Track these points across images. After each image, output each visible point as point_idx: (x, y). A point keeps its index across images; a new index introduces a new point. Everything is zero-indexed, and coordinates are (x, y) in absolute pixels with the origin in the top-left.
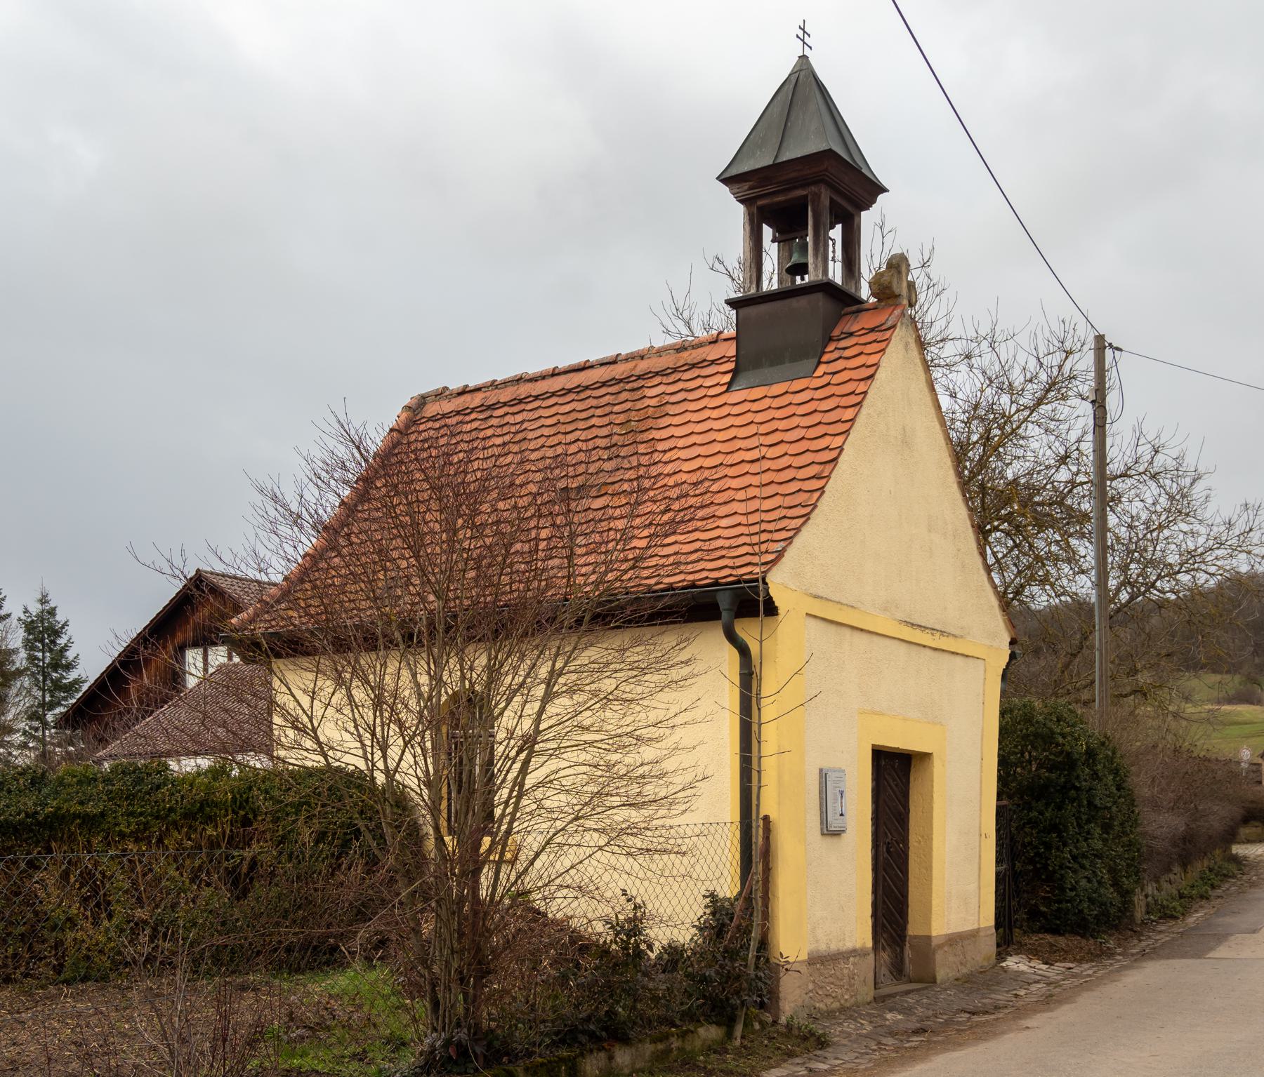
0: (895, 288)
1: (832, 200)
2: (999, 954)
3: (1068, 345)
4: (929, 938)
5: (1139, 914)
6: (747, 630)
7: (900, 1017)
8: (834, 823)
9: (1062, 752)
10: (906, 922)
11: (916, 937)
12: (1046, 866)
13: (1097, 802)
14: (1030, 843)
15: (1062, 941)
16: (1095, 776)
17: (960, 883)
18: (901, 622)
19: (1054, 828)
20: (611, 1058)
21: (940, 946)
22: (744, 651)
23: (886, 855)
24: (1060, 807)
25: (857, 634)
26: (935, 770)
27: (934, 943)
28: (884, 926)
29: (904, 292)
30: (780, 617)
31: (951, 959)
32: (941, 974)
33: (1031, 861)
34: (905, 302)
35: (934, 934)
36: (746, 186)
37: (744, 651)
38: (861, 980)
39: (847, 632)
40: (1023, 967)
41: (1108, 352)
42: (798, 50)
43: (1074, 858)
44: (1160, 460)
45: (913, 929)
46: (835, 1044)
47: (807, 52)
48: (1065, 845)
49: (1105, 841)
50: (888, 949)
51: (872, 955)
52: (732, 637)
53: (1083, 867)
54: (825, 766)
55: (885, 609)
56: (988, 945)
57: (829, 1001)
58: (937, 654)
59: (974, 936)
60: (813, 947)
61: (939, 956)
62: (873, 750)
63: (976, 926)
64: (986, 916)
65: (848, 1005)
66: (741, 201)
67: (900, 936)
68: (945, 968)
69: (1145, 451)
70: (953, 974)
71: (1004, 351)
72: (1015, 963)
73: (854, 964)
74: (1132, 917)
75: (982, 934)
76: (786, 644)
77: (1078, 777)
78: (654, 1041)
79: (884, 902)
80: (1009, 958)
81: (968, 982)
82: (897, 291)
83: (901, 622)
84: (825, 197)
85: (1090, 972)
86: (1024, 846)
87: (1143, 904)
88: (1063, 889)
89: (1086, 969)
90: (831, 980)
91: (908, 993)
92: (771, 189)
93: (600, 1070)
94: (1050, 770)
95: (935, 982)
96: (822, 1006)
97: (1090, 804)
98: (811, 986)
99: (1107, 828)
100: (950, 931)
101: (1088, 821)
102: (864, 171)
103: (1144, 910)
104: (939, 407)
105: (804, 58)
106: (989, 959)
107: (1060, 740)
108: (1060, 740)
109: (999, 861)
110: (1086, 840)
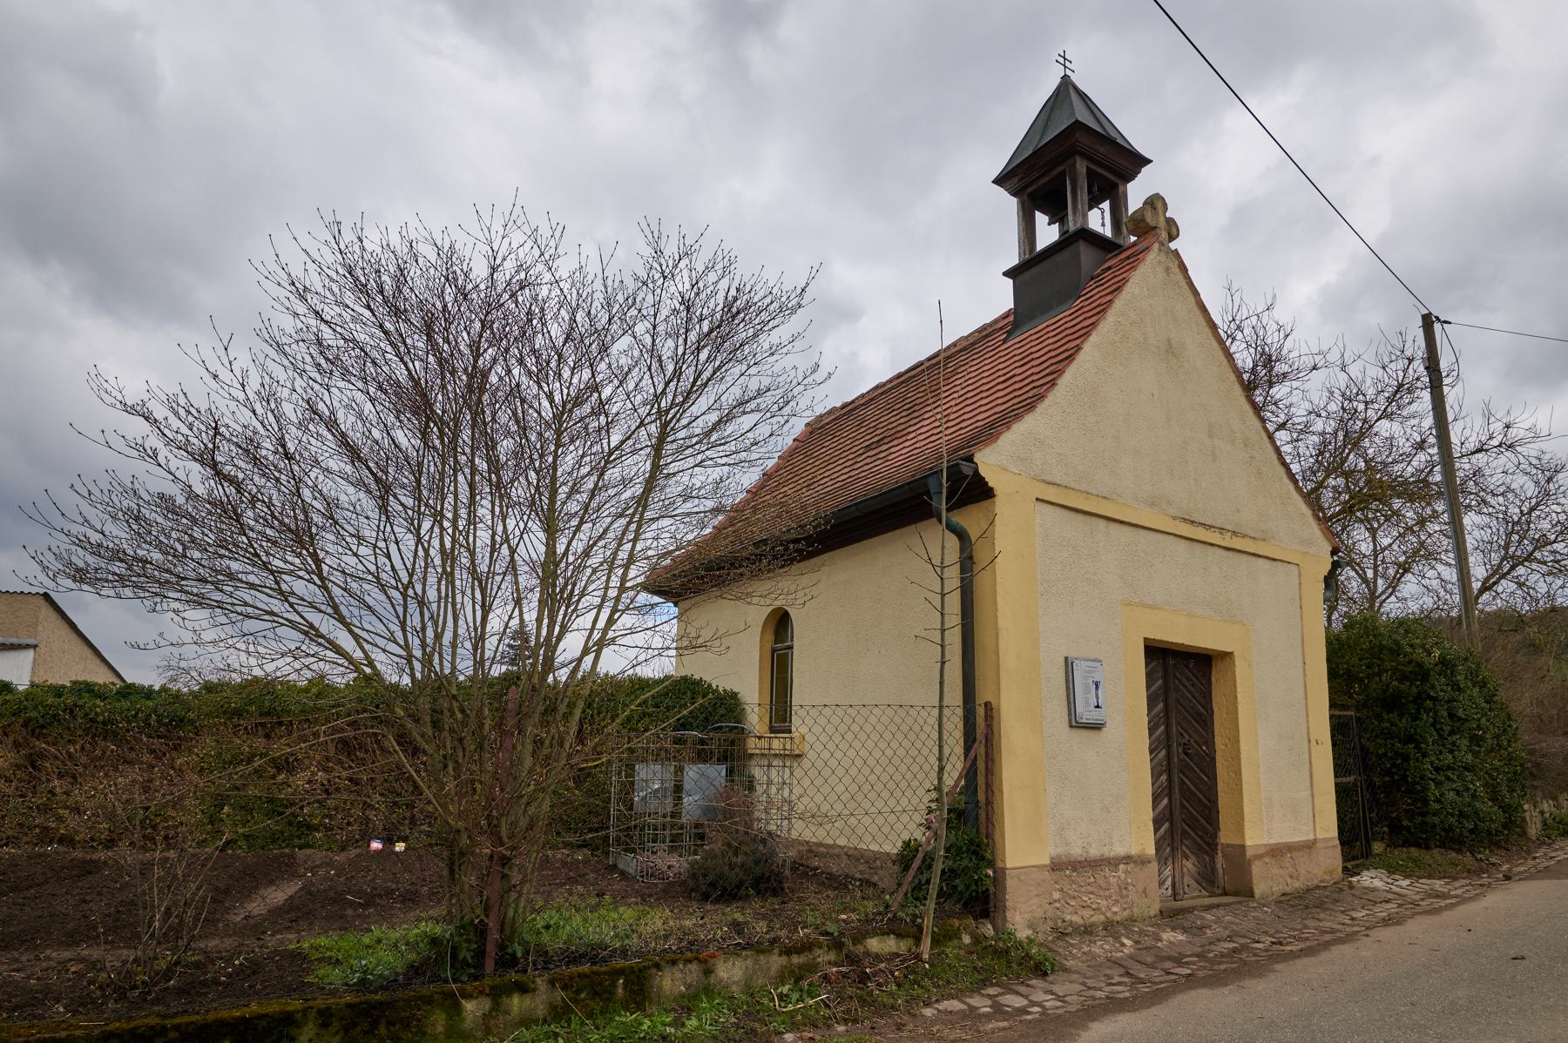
0: (1154, 226)
1: (1090, 172)
2: (1345, 869)
3: (1408, 353)
4: (1243, 847)
5: (1534, 829)
6: (970, 519)
7: (1181, 937)
8: (1086, 713)
9: (1410, 662)
10: (1217, 828)
11: (1229, 846)
12: (1404, 778)
13: (1461, 713)
14: (1385, 755)
15: (1426, 856)
16: (1457, 688)
17: (1285, 786)
18: (1175, 518)
19: (1410, 739)
20: (708, 972)
21: (1259, 857)
22: (962, 535)
23: (1183, 756)
24: (1416, 718)
25: (1114, 527)
26: (1238, 670)
27: (1249, 853)
28: (1184, 832)
29: (1162, 224)
30: (997, 499)
31: (1276, 871)
32: (1260, 888)
33: (1388, 773)
34: (1164, 235)
35: (1248, 843)
36: (1015, 180)
37: (962, 535)
38: (1146, 892)
39: (1102, 523)
40: (1377, 883)
41: (1437, 326)
42: (1059, 72)
43: (1437, 770)
44: (1513, 432)
45: (1225, 837)
46: (1066, 970)
47: (1069, 73)
48: (1425, 755)
49: (1476, 754)
50: (1193, 858)
51: (1154, 866)
52: (953, 528)
53: (1448, 779)
54: (1072, 655)
55: (1153, 504)
56: (1330, 860)
57: (1087, 913)
58: (1231, 554)
59: (1309, 847)
60: (1060, 850)
61: (1256, 869)
62: (1146, 647)
63: (1311, 837)
64: (1328, 826)
65: (1118, 918)
66: (1014, 195)
67: (1208, 844)
68: (1266, 881)
69: (1497, 427)
70: (1278, 888)
71: (1354, 370)
72: (1371, 879)
73: (1126, 872)
74: (1524, 833)
75: (1319, 845)
76: (1016, 530)
77: (1433, 687)
78: (788, 952)
79: (1183, 806)
80: (1365, 873)
81: (1304, 901)
82: (1153, 224)
83: (1175, 518)
84: (1081, 166)
85: (1459, 892)
86: (1379, 757)
87: (1538, 820)
88: (1426, 802)
89: (1458, 888)
90: (1090, 889)
91: (1209, 908)
92: (1036, 174)
93: (689, 987)
94: (1401, 682)
95: (1251, 894)
96: (1075, 918)
97: (1452, 716)
98: (1056, 895)
99: (1476, 740)
100: (1272, 841)
101: (1452, 733)
102: (1120, 141)
103: (1539, 826)
104: (1213, 326)
105: (1065, 77)
106: (1331, 872)
107: (1408, 649)
108: (1408, 649)
109: (1340, 768)
110: (1451, 752)
